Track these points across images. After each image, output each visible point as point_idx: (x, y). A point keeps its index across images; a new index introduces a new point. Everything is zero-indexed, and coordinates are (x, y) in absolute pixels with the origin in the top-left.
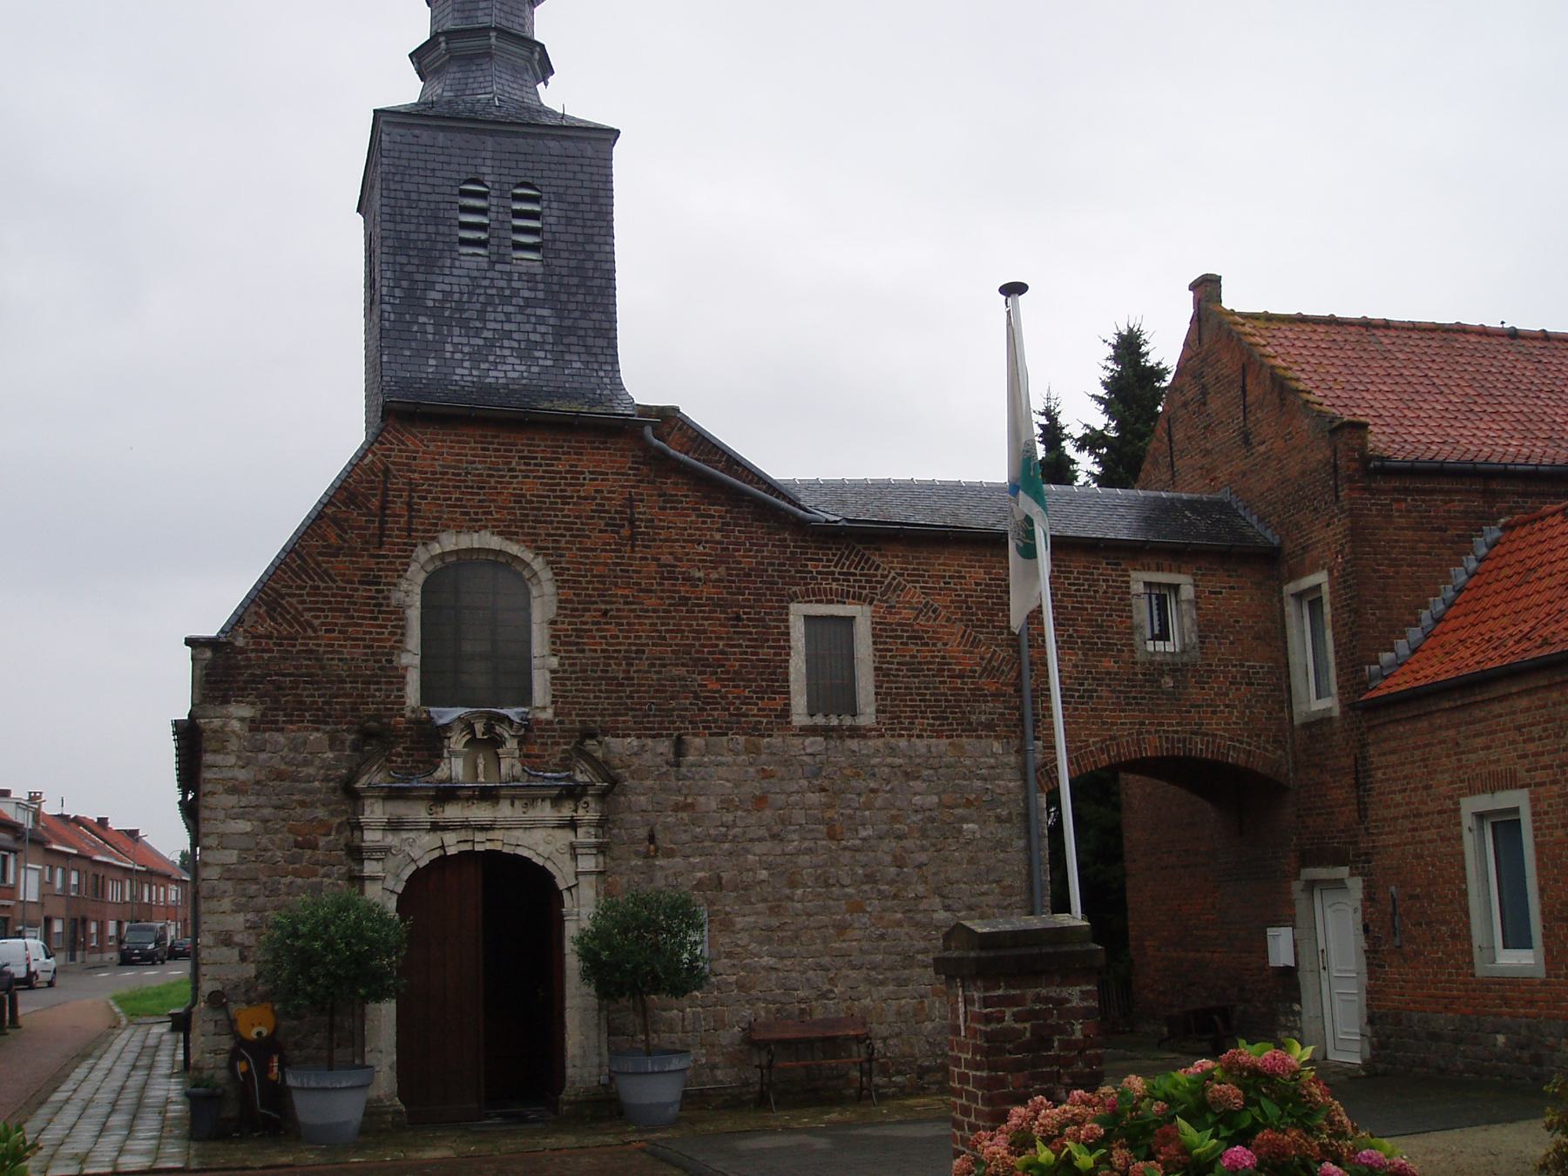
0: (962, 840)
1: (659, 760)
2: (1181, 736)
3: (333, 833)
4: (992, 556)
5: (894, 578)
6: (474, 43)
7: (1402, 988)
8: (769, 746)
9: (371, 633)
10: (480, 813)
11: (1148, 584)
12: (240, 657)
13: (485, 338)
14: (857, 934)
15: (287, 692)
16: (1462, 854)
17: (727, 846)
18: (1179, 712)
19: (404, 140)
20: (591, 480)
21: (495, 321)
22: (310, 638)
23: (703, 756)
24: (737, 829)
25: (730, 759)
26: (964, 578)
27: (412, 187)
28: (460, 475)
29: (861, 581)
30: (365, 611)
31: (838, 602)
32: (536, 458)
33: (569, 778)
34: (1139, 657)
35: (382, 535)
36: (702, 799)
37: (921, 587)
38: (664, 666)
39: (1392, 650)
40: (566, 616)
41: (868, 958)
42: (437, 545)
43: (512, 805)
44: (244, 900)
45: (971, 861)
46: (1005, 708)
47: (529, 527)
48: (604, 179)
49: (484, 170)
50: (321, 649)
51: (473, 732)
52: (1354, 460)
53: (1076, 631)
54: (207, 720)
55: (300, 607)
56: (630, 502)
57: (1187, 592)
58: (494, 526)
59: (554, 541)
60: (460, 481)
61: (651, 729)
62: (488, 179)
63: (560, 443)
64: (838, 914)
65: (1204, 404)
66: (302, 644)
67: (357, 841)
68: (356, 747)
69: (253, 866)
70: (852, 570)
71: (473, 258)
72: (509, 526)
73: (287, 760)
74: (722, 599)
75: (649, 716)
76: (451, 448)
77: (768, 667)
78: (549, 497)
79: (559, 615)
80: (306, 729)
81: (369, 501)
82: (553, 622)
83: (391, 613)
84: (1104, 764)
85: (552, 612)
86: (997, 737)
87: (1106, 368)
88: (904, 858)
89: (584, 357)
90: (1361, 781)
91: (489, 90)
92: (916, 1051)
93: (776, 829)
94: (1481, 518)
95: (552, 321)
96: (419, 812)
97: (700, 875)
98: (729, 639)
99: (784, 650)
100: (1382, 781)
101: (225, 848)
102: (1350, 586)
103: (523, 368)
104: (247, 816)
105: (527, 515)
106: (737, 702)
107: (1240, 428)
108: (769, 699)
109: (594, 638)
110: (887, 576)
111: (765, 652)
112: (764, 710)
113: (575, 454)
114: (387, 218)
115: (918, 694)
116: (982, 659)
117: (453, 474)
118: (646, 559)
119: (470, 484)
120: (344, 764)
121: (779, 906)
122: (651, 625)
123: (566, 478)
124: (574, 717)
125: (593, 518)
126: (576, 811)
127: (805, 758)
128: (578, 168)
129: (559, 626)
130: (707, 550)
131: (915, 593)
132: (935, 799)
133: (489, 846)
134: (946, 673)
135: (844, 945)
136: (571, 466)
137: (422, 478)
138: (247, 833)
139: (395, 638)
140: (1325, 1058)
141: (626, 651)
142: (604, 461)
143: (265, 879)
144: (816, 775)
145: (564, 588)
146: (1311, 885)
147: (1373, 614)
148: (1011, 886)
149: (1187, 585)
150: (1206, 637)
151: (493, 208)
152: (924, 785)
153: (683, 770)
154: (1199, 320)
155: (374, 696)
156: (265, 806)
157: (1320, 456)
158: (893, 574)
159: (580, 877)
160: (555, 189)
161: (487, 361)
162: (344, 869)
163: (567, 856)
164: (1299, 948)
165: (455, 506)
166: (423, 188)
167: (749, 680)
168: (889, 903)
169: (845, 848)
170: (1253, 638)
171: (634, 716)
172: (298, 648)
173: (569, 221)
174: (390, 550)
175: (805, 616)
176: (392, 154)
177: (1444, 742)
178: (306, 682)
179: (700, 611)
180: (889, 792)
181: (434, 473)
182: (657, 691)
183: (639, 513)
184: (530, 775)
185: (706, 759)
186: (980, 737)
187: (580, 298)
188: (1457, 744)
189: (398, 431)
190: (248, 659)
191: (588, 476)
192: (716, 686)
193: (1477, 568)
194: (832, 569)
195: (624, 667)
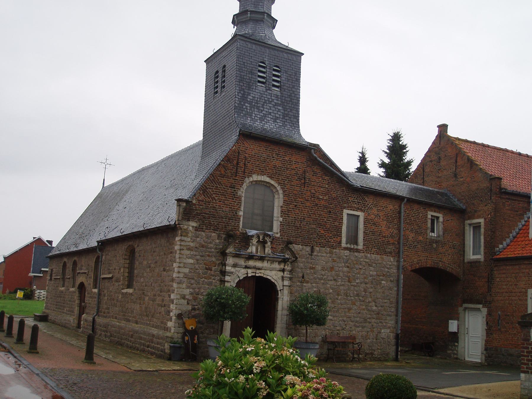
0: (381, 286)
1: (307, 253)
2: (437, 261)
3: (217, 266)
4: (395, 202)
5: (370, 205)
6: (260, 16)
7: (499, 341)
8: (335, 252)
9: (231, 203)
10: (259, 264)
11: (432, 216)
12: (194, 206)
13: (264, 114)
14: (353, 311)
15: (207, 219)
16: (527, 305)
17: (322, 281)
18: (437, 254)
19: (244, 45)
20: (295, 164)
21: (266, 108)
22: (214, 203)
23: (318, 253)
24: (325, 277)
25: (325, 255)
26: (387, 207)
27: (245, 61)
28: (259, 157)
29: (362, 205)
30: (230, 196)
31: (356, 211)
32: (280, 155)
33: (284, 256)
34: (428, 237)
35: (236, 173)
36: (317, 266)
37: (377, 209)
38: (310, 224)
39: (502, 244)
40: (285, 205)
41: (356, 319)
42: (252, 178)
43: (268, 262)
44: (189, 285)
45: (383, 293)
46: (395, 248)
47: (277, 176)
48: (298, 68)
49: (265, 59)
50: (217, 207)
51: (259, 238)
52: (497, 188)
53: (414, 227)
54: (183, 226)
55: (212, 193)
56: (305, 172)
57: (441, 219)
58: (268, 174)
59: (284, 181)
60: (259, 159)
61: (305, 243)
62: (267, 62)
63: (287, 151)
64: (349, 305)
65: (439, 162)
66: (212, 205)
67: (223, 270)
68: (225, 240)
69: (193, 274)
70: (360, 201)
71: (262, 87)
72: (271, 175)
73: (205, 241)
74: (326, 206)
75: (305, 239)
76: (257, 148)
77: (337, 228)
78: (283, 167)
79: (283, 205)
80: (211, 232)
81: (233, 161)
82: (282, 207)
83: (238, 198)
84: (417, 267)
85: (281, 203)
86: (392, 256)
87: (389, 143)
88: (366, 289)
89: (290, 124)
90: (490, 280)
91: (264, 33)
92: (365, 348)
93: (335, 277)
94: (526, 209)
95: (282, 111)
96: (242, 262)
97: (315, 289)
98: (328, 218)
99: (341, 223)
100: (498, 281)
101: (185, 268)
102: (492, 224)
103: (274, 125)
104: (192, 258)
105: (277, 172)
106: (328, 238)
107: (453, 172)
108: (336, 238)
109: (292, 213)
110: (369, 204)
111: (337, 224)
112: (335, 241)
113: (291, 155)
114: (238, 70)
115: (374, 241)
116: (390, 232)
117: (257, 156)
118: (307, 190)
119: (262, 160)
120: (221, 244)
121: (334, 301)
122: (308, 211)
123: (288, 162)
124: (285, 237)
125: (294, 176)
126: (285, 266)
127: (344, 257)
128: (291, 64)
129: (283, 208)
130: (324, 190)
131: (375, 211)
132: (375, 273)
133: (260, 275)
134: (381, 236)
135: (350, 314)
136: (290, 159)
137: (248, 156)
138: (192, 263)
139: (238, 206)
140: (464, 359)
141: (300, 218)
142: (298, 158)
143: (196, 279)
144: (346, 263)
145: (285, 196)
146: (465, 309)
147: (499, 233)
148: (392, 301)
149: (440, 216)
150: (445, 233)
151: (267, 72)
152: (373, 268)
153: (313, 257)
154: (440, 137)
155: (231, 224)
156: (198, 255)
157: (485, 185)
158: (370, 204)
159: (284, 287)
160: (285, 69)
161: (264, 121)
162: (219, 278)
163: (281, 280)
164: (459, 327)
165: (257, 166)
166: (249, 62)
167: (332, 231)
168: (362, 303)
169: (352, 285)
170: (456, 235)
171: (301, 239)
172: (211, 206)
173: (288, 80)
174: (239, 178)
175: (347, 214)
176: (240, 49)
177: (524, 273)
178: (212, 217)
179: (321, 209)
180: (364, 269)
181: (252, 155)
182: (307, 232)
183: (307, 176)
184: (273, 254)
185: (319, 254)
186: (388, 256)
187: (290, 105)
188: (529, 274)
189: (242, 140)
190: (196, 207)
191: (294, 162)
192: (323, 232)
193: (525, 224)
194: (355, 200)
195: (299, 223)
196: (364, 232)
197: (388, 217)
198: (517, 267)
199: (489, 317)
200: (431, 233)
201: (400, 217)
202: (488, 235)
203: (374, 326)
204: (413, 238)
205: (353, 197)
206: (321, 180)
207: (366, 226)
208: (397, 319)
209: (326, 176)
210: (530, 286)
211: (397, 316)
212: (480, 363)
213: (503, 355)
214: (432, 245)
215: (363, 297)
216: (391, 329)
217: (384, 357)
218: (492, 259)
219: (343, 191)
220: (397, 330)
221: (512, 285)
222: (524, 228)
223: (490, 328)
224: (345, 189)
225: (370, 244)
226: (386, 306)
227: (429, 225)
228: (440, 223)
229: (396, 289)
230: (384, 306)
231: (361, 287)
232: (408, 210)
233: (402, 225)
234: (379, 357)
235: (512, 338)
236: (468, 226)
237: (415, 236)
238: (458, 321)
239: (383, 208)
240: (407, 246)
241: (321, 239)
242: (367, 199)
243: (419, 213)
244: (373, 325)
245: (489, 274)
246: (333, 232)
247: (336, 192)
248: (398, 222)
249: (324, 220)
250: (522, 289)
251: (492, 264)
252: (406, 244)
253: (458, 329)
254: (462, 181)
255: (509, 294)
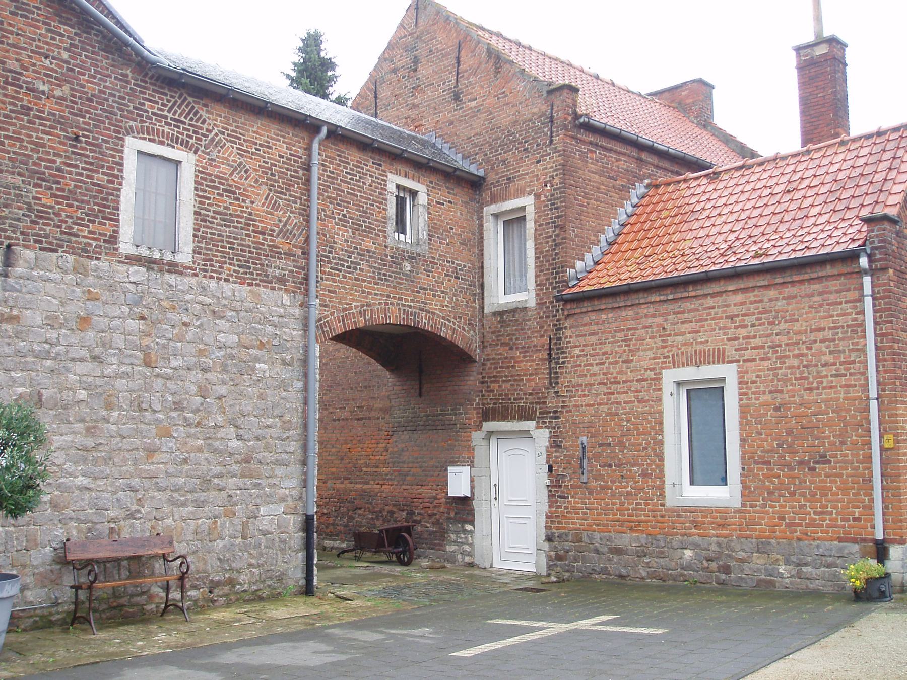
2: (414, 310)
5: (216, 135)
7: (585, 514)
8: (97, 269)
11: (398, 187)
14: (164, 457)
16: (661, 413)
17: (49, 363)
18: (412, 291)
29: (189, 130)
31: (168, 145)
36: (28, 313)
37: (238, 149)
39: (583, 260)
41: (172, 480)
45: (261, 397)
53: (349, 212)
57: (422, 198)
65: (415, 70)
70: (182, 119)
77: (101, 192)
86: (287, 291)
93: (97, 351)
97: (21, 390)
106: (70, 221)
108: (100, 223)
110: (210, 131)
111: (100, 178)
116: (280, 221)
121: (94, 427)
130: (53, 66)
134: (251, 228)
144: (137, 304)
147: (574, 231)
153: (11, 281)
157: (535, 110)
158: (216, 131)
164: (476, 483)
167: (82, 201)
168: (193, 430)
169: (157, 376)
179: (41, 125)
180: (198, 327)
186: (273, 288)
188: (664, 328)
194: (166, 113)
196: (196, 213)
197: (272, 174)
198: (630, 313)
199: (556, 451)
200: (396, 234)
201: (308, 181)
202: (547, 237)
203: (235, 499)
204: (347, 241)
205: (157, 103)
206: (43, 32)
207: (201, 194)
208: (305, 474)
209: (64, 24)
210: (669, 362)
211: (304, 463)
212: (536, 576)
213: (597, 551)
214: (400, 264)
215: (195, 411)
216: (290, 501)
217: (269, 586)
218: (559, 299)
219: (124, 79)
220: (305, 507)
221: (616, 362)
222: (632, 220)
223: (558, 481)
224: (130, 75)
225: (217, 251)
226: (271, 437)
227: (392, 210)
228: (421, 209)
229: (300, 385)
230: (264, 438)
231: (187, 383)
232: (331, 163)
233: (315, 204)
234: (255, 588)
235: (622, 504)
236: (491, 218)
237: (354, 238)
238: (472, 466)
239: (256, 149)
240: (330, 263)
241: (44, 224)
242: (205, 115)
243: (363, 174)
244: (230, 496)
245: (550, 339)
246: (88, 203)
247: (100, 79)
248: (302, 194)
249: (54, 162)
250: (646, 370)
251: (558, 311)
252: (328, 257)
253: (472, 488)
254: (475, 107)
255: (610, 388)
